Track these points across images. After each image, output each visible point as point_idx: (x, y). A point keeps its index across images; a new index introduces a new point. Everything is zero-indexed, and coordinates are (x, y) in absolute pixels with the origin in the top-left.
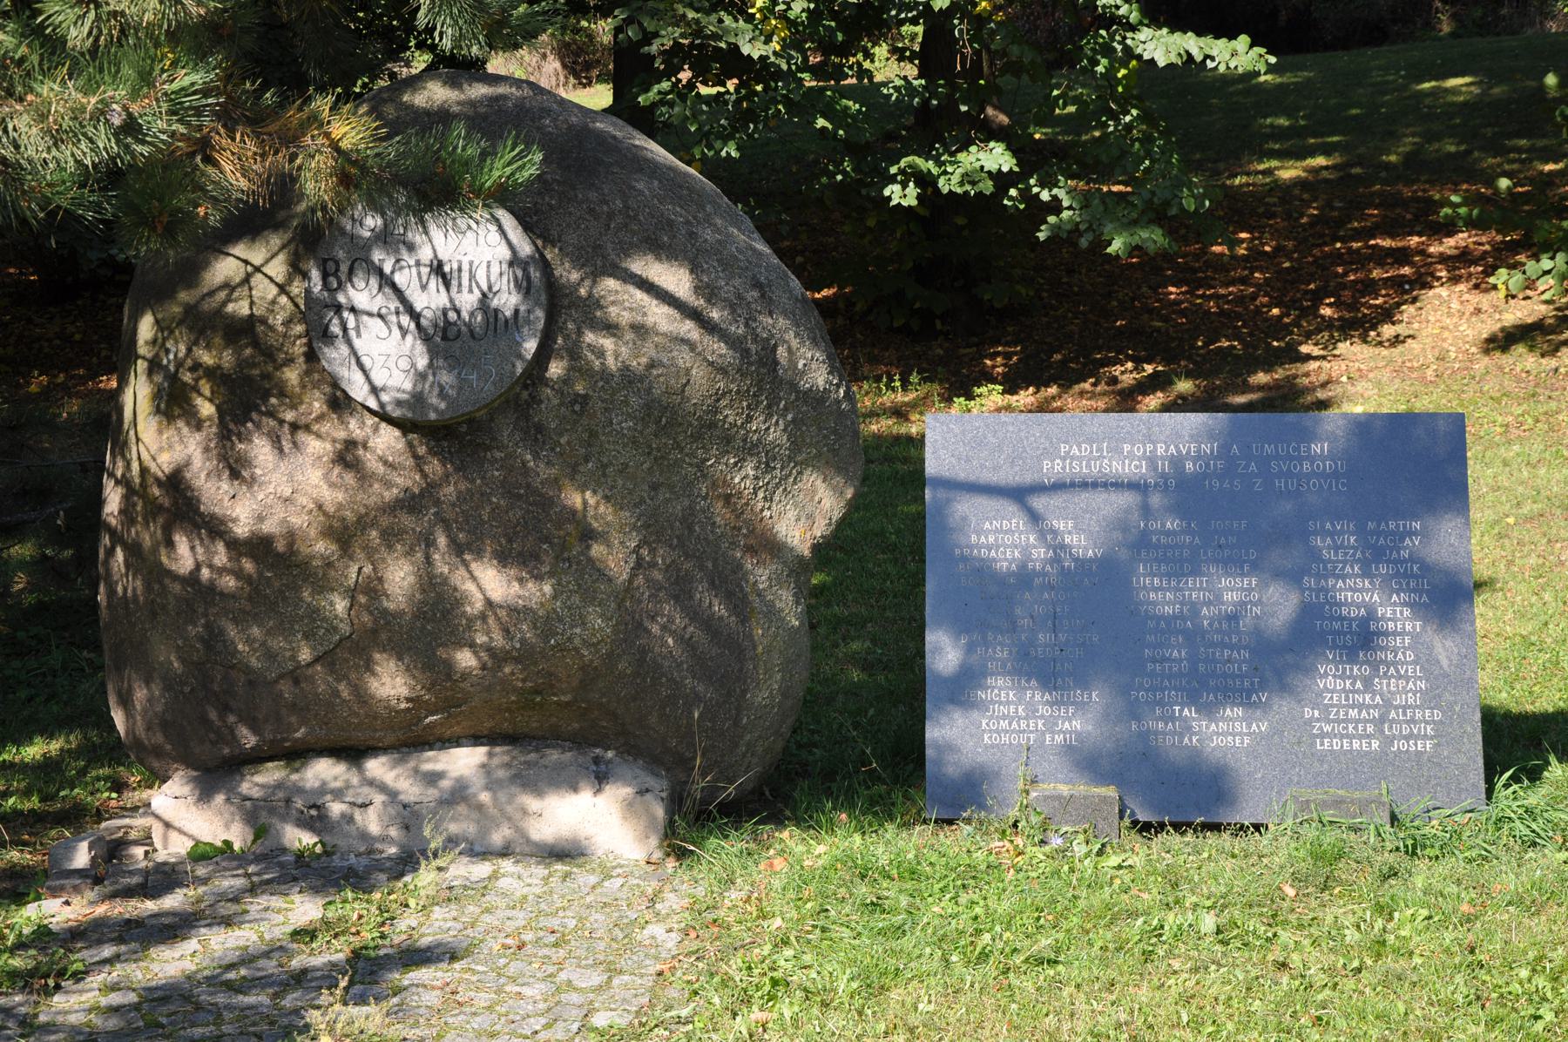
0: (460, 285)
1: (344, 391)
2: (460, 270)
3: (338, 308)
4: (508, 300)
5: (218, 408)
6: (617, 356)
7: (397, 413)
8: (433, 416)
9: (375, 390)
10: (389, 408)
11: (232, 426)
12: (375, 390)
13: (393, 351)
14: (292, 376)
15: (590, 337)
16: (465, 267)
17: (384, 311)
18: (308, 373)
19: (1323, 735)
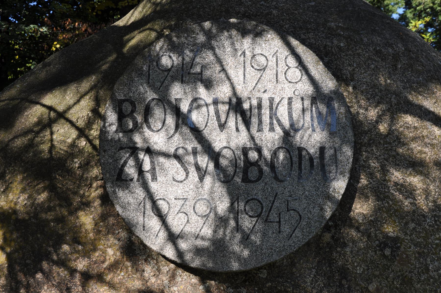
0: (260, 122)
1: (138, 237)
2: (260, 106)
3: (134, 150)
4: (312, 138)
5: (9, 257)
6: (427, 193)
7: (196, 263)
8: (235, 266)
9: (173, 238)
10: (188, 257)
11: (21, 277)
12: (173, 238)
13: (191, 195)
14: (87, 220)
15: (396, 175)
16: (266, 103)
17: (181, 151)
18: (103, 217)
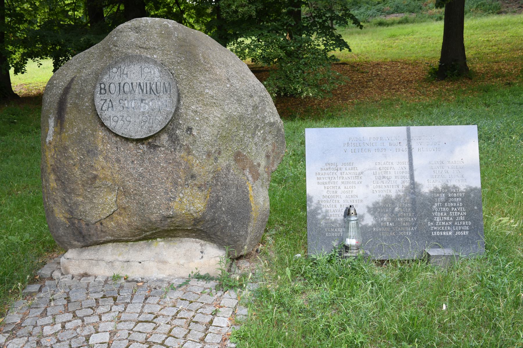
19: (434, 231)
